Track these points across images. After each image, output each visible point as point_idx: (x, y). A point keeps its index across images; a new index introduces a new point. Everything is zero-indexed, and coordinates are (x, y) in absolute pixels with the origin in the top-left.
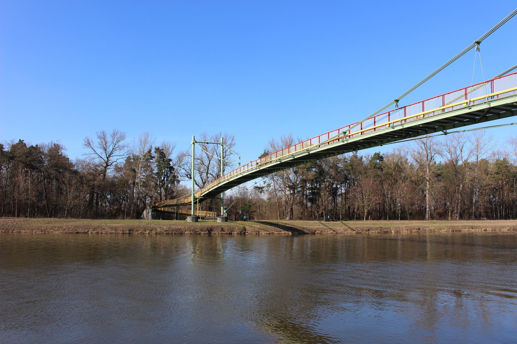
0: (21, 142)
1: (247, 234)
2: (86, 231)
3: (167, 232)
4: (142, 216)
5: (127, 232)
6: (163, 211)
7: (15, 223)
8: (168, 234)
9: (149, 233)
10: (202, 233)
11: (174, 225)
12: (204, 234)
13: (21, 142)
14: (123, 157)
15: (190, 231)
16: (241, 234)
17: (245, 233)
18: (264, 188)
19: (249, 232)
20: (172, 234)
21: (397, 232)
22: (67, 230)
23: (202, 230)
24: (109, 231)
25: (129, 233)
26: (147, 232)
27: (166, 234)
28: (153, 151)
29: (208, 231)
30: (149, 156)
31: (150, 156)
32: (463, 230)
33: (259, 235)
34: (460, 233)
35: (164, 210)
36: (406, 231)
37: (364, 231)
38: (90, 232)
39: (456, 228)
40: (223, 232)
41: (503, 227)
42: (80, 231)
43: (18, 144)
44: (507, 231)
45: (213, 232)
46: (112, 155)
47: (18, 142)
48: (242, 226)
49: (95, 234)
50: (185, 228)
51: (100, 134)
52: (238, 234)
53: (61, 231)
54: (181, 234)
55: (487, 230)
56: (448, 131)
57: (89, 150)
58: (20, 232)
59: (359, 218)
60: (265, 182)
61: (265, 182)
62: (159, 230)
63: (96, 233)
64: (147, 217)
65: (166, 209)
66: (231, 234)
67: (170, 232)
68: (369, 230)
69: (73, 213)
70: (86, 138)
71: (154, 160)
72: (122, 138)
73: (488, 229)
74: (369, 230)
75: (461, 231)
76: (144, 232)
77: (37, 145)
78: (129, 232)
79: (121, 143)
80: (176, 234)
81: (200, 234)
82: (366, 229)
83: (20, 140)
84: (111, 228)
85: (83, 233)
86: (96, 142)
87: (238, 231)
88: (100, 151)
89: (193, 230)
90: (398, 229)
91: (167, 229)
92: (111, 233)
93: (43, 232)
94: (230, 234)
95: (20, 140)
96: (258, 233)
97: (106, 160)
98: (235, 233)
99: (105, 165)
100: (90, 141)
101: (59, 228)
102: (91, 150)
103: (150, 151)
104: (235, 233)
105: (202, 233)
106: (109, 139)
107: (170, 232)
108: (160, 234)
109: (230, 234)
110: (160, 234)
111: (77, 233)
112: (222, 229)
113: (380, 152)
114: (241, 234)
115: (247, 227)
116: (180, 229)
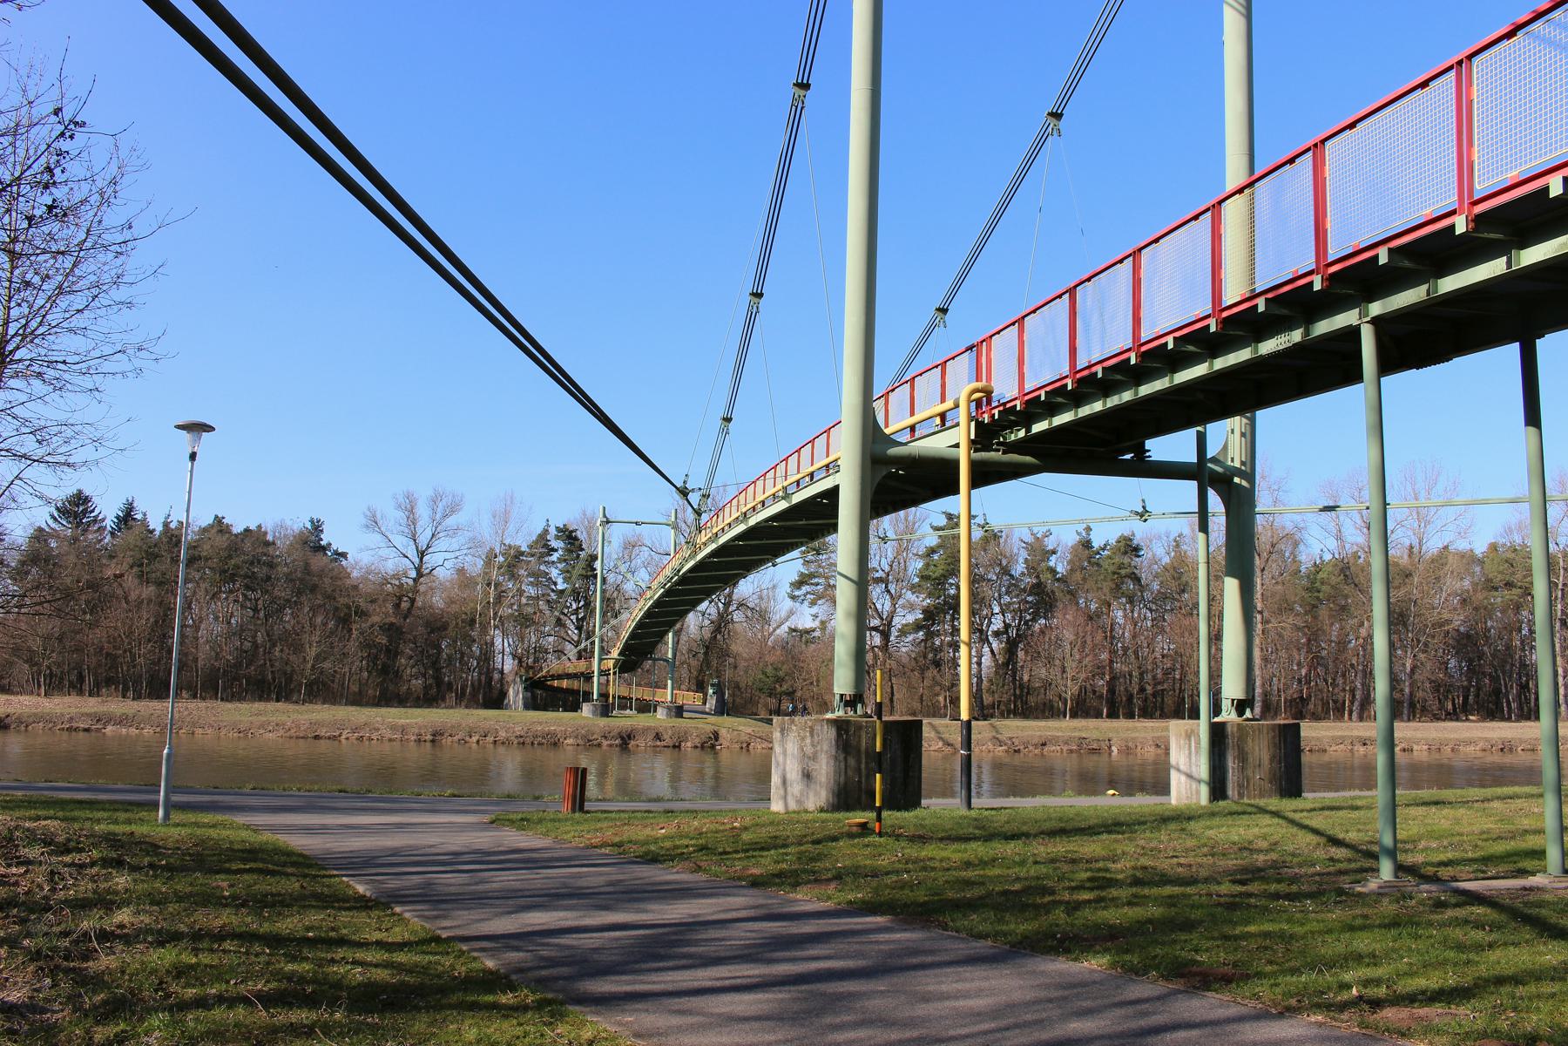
0: (219, 520)
1: (718, 747)
2: (337, 734)
3: (521, 740)
4: (506, 701)
5: (429, 737)
6: (567, 689)
7: (186, 713)
8: (523, 743)
9: (478, 742)
10: (605, 743)
11: (541, 723)
12: (611, 746)
13: (219, 520)
14: (458, 554)
15: (576, 737)
16: (702, 747)
17: (713, 747)
18: (813, 631)
19: (725, 744)
20: (532, 743)
21: (1127, 751)
22: (293, 731)
23: (606, 737)
24: (388, 734)
25: (433, 741)
26: (475, 739)
27: (519, 743)
28: (553, 531)
29: (622, 738)
30: (542, 546)
31: (546, 546)
32: (1334, 748)
33: (748, 750)
34: (1326, 758)
35: (570, 687)
36: (1152, 749)
37: (1031, 748)
38: (344, 737)
39: (1313, 743)
40: (658, 743)
41: (1469, 742)
42: (323, 734)
43: (211, 526)
44: (1480, 754)
45: (632, 742)
46: (430, 550)
47: (211, 522)
48: (709, 728)
49: (355, 742)
50: (566, 730)
51: (401, 500)
52: (696, 747)
53: (281, 732)
54: (555, 744)
55: (1412, 750)
56: (778, 560)
57: (375, 539)
58: (193, 733)
59: (1049, 711)
60: (815, 616)
61: (815, 616)
62: (502, 734)
63: (357, 739)
64: (515, 702)
65: (565, 684)
66: (679, 747)
67: (528, 741)
68: (1044, 744)
69: (322, 690)
70: (369, 509)
71: (555, 557)
72: (453, 509)
73: (1415, 747)
74: (1044, 744)
75: (1325, 751)
76: (467, 739)
77: (260, 527)
78: (431, 738)
79: (451, 521)
80: (543, 744)
81: (599, 745)
82: (1036, 741)
83: (216, 517)
84: (393, 728)
85: (329, 738)
86: (393, 517)
87: (697, 740)
88: (401, 541)
89: (584, 737)
90: (1130, 744)
91: (522, 733)
92: (390, 740)
93: (241, 735)
94: (677, 747)
95: (216, 517)
96: (744, 745)
97: (417, 561)
98: (689, 744)
99: (413, 574)
100: (379, 516)
101: (277, 725)
102: (379, 537)
103: (546, 532)
104: (689, 744)
105: (605, 743)
106: (423, 512)
107: (528, 741)
108: (503, 743)
109: (674, 747)
110: (503, 743)
111: (317, 737)
112: (657, 734)
113: (1133, 535)
114: (702, 747)
115: (723, 732)
116: (554, 734)
